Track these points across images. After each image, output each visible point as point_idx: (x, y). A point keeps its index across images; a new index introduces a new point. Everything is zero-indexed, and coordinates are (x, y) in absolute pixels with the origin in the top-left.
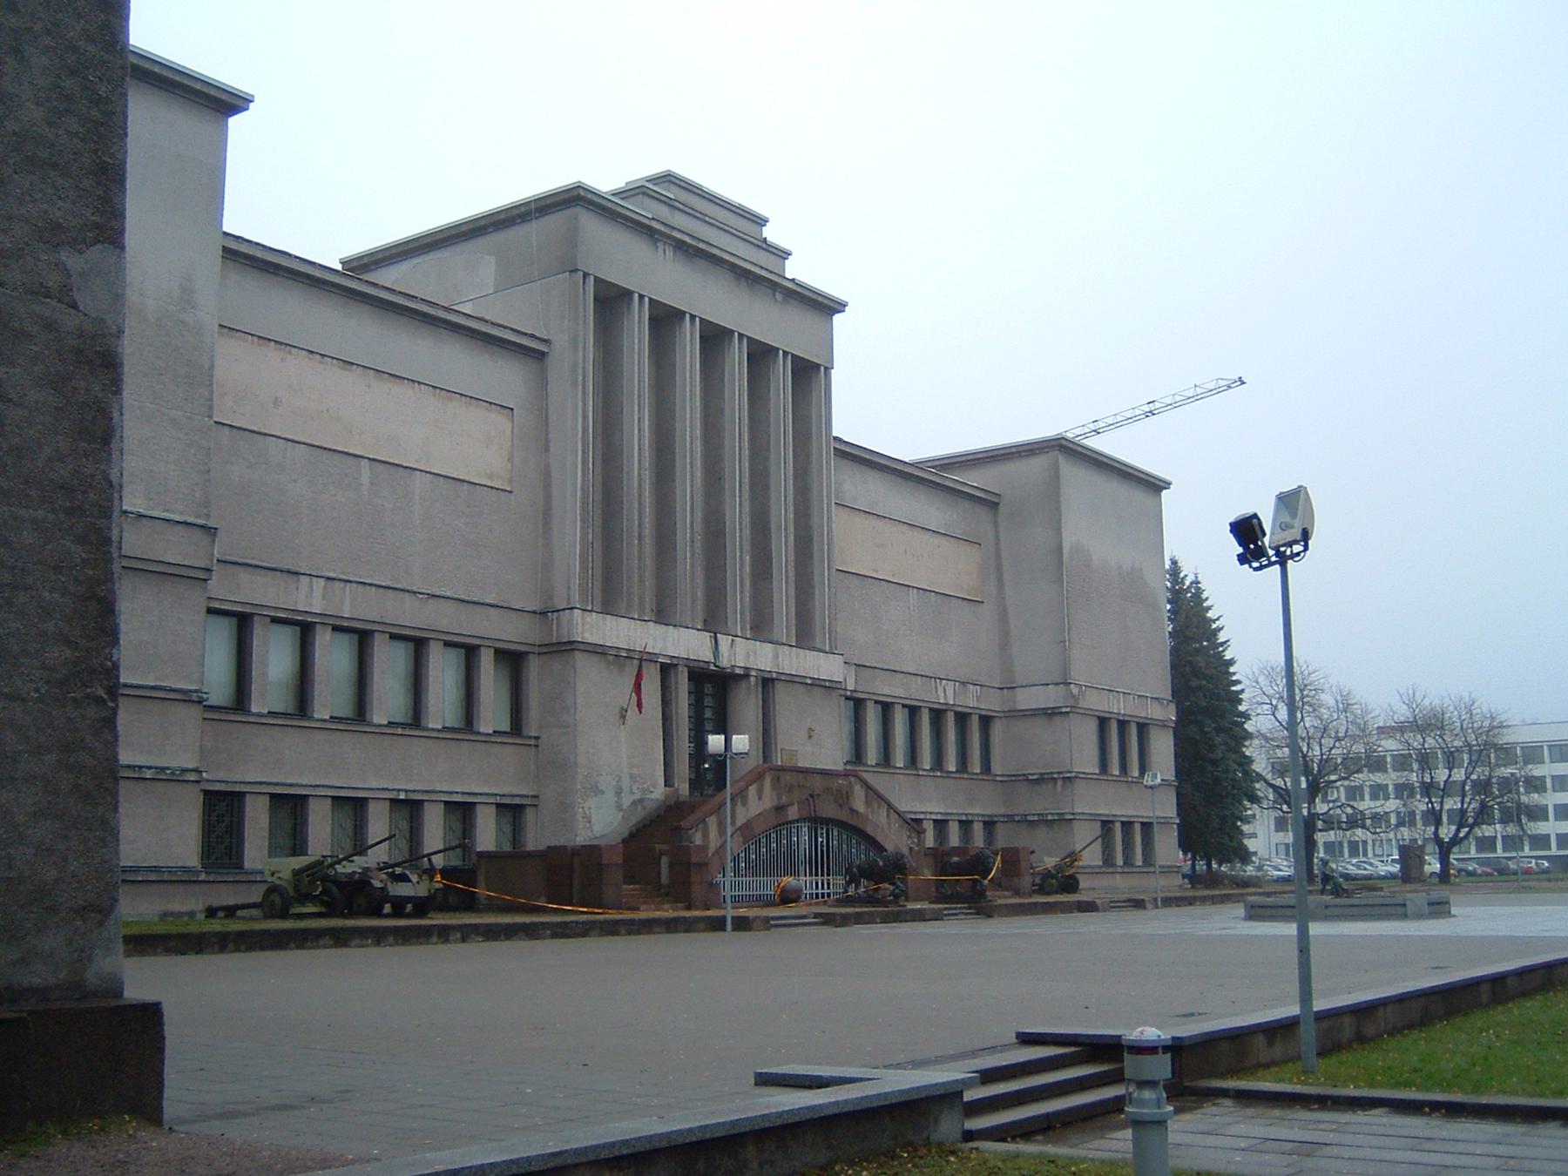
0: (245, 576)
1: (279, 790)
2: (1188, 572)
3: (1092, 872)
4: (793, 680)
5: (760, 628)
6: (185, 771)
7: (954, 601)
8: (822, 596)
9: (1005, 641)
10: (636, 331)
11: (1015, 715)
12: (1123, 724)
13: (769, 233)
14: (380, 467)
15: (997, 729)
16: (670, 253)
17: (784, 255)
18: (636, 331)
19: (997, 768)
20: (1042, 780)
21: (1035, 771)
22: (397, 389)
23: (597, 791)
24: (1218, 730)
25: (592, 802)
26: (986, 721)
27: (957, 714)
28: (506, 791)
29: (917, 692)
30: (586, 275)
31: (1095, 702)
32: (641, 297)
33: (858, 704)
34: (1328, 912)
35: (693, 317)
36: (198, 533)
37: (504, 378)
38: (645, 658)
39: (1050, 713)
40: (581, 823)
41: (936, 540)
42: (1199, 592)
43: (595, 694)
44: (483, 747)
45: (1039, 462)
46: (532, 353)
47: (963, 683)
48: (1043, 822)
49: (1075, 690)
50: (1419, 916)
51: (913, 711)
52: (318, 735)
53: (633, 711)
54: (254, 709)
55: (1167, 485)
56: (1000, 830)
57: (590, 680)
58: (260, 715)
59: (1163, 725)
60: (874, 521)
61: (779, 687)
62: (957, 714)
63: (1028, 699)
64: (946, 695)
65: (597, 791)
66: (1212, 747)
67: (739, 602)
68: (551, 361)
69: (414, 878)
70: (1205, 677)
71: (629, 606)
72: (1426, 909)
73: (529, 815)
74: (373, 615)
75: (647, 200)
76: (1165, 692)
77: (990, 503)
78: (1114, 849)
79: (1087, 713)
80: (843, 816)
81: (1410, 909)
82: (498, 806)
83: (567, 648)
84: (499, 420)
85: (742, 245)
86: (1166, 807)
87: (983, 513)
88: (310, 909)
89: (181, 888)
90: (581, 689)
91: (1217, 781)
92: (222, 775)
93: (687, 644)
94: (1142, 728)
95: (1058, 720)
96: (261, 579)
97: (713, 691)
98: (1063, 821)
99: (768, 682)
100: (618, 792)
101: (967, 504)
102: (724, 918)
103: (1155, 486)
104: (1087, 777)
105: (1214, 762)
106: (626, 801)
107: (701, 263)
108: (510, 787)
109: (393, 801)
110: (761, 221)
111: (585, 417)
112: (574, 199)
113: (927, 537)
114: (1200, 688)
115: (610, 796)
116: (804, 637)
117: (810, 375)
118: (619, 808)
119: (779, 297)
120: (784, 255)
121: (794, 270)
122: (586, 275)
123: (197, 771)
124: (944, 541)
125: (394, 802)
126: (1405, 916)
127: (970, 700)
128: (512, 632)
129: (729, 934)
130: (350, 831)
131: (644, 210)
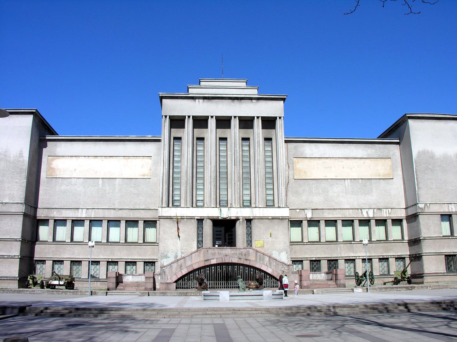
0: (64, 211)
14: (105, 180)
22: (111, 160)
122: (166, 116)
124: (368, 161)
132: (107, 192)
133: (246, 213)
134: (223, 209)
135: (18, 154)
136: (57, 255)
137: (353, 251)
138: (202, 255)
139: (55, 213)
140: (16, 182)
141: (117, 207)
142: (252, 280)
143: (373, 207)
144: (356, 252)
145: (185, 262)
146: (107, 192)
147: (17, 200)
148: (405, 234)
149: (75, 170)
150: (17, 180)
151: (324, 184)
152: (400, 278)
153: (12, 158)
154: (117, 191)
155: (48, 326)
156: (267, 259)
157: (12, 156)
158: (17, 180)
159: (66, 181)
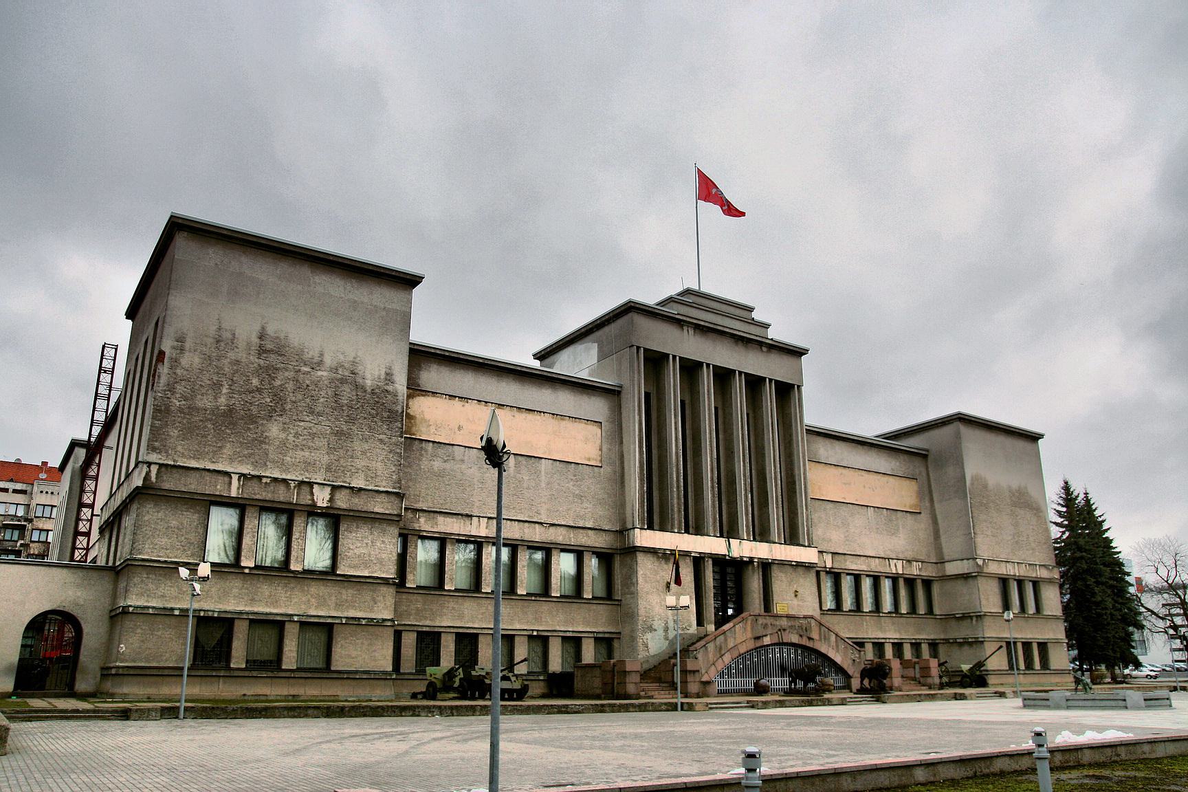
0: (440, 519)
1: (461, 631)
2: (1078, 489)
3: (999, 673)
4: (783, 564)
5: (761, 534)
6: (384, 620)
7: (900, 514)
8: (803, 513)
9: (937, 535)
10: (673, 378)
11: (945, 578)
12: (1020, 583)
13: (756, 315)
14: (520, 458)
15: (936, 589)
16: (691, 332)
17: (766, 326)
18: (673, 378)
19: (937, 611)
20: (965, 617)
21: (959, 612)
22: (530, 416)
23: (651, 629)
24: (1098, 583)
25: (649, 636)
26: (927, 583)
27: (923, 581)
28: (601, 630)
29: (876, 566)
30: (638, 348)
31: (993, 568)
32: (674, 357)
33: (836, 577)
34: (1070, 703)
35: (708, 365)
36: (393, 498)
37: (597, 407)
38: (686, 554)
39: (966, 577)
40: (641, 647)
41: (886, 478)
42: (1087, 501)
43: (648, 574)
44: (520, 603)
45: (947, 431)
46: (612, 394)
47: (909, 561)
48: (966, 643)
49: (980, 562)
50: (1058, 707)
51: (876, 580)
52: (484, 601)
53: (673, 585)
54: (519, 592)
55: (1041, 436)
56: (942, 650)
57: (645, 566)
58: (449, 591)
59: (1050, 581)
60: (841, 470)
61: (774, 568)
62: (923, 581)
63: (952, 569)
64: (898, 568)
65: (651, 629)
66: (1094, 594)
67: (744, 522)
68: (623, 395)
69: (513, 679)
70: (1086, 551)
71: (673, 526)
72: (1064, 703)
73: (616, 644)
74: (517, 536)
75: (675, 305)
76: (1051, 561)
77: (922, 455)
78: (1032, 660)
79: (990, 576)
80: (804, 642)
81: (1129, 703)
82: (596, 639)
83: (633, 551)
84: (595, 430)
85: (734, 322)
86: (1056, 632)
87: (918, 462)
88: (452, 695)
89: (382, 682)
90: (640, 572)
91: (1100, 615)
92: (428, 623)
93: (712, 545)
94: (1036, 584)
95: (970, 581)
96: (449, 520)
97: (731, 573)
98: (978, 643)
99: (766, 566)
100: (666, 629)
101: (906, 457)
102: (178, 708)
103: (1034, 438)
104: (993, 615)
105: (1098, 604)
106: (671, 634)
107: (711, 335)
108: (602, 627)
109: (564, 638)
110: (751, 310)
111: (640, 424)
112: (630, 308)
113: (879, 476)
114: (1082, 558)
115: (661, 632)
116: (792, 538)
117: (787, 392)
118: (666, 638)
119: (764, 349)
120: (766, 326)
121: (773, 334)
122: (638, 348)
123: (392, 620)
124: (891, 479)
125: (530, 637)
126: (1048, 707)
127: (915, 570)
128: (929, 572)
129: (679, 713)
130: (540, 654)
131: (673, 310)
132: (525, 485)
133: (761, 551)
134: (734, 542)
135: (383, 373)
136: (426, 618)
137: (881, 629)
138: (749, 628)
139: (422, 520)
140: (381, 441)
141: (543, 519)
142: (1029, 665)
143: (901, 556)
144: (885, 631)
145: (726, 640)
146: (525, 485)
147: (384, 483)
148: (275, 603)
149: (460, 428)
150: (381, 437)
151: (844, 510)
152: (439, 685)
153: (369, 383)
154: (543, 485)
155: (1125, 735)
156: (833, 638)
157: (368, 376)
158: (381, 437)
159: (441, 451)
